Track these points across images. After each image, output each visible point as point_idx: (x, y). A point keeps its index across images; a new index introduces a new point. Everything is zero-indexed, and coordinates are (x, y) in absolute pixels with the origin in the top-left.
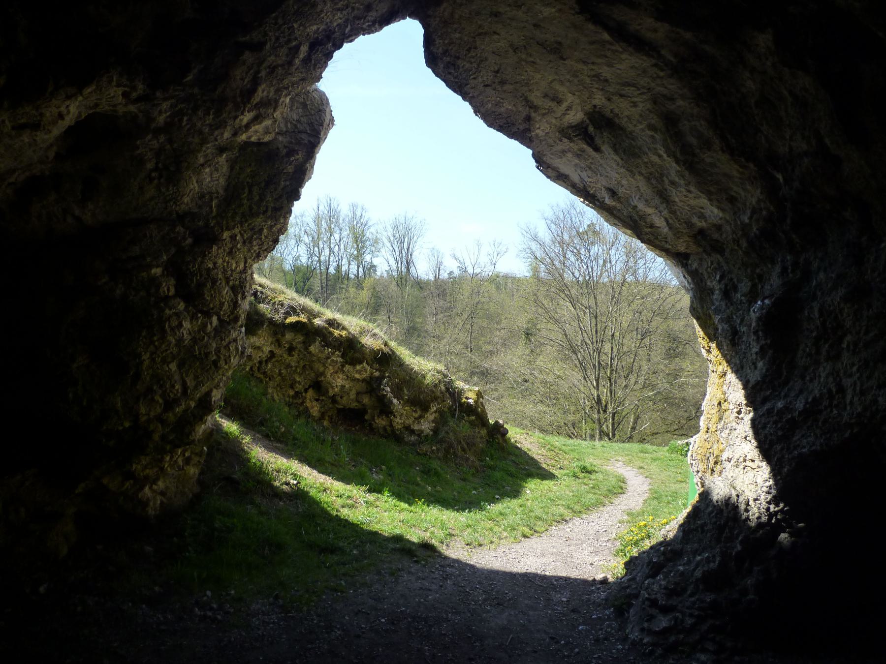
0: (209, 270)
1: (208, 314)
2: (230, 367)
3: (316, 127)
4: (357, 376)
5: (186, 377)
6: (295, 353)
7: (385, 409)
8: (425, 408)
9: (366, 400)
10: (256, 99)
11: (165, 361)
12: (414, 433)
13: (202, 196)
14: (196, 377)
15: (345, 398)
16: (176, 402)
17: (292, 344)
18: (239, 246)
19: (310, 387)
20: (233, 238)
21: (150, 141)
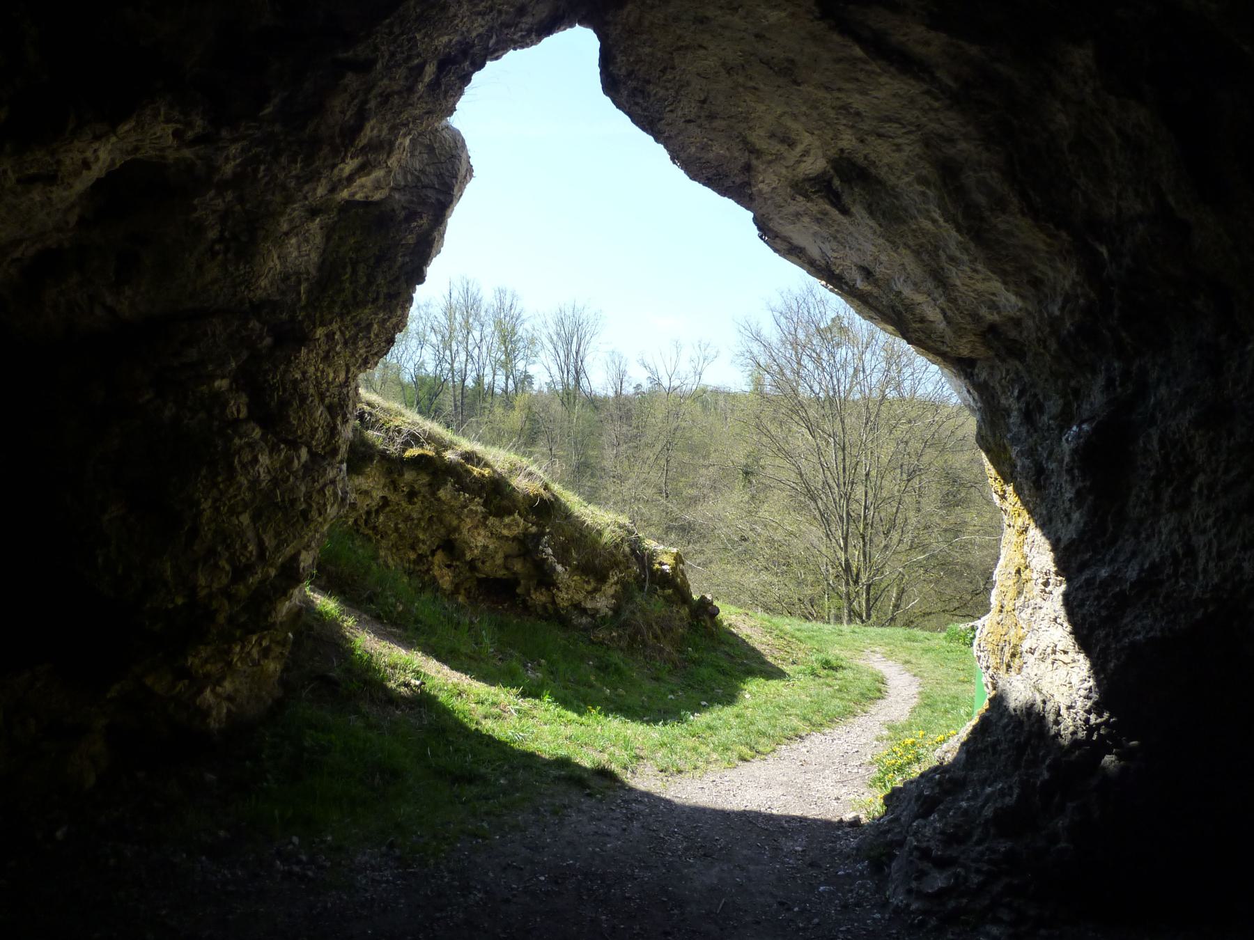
0: (295, 382)
1: (294, 445)
2: (325, 520)
3: (447, 180)
4: (505, 532)
6: (418, 500)
7: (545, 579)
8: (602, 578)
9: (518, 566)
10: (362, 140)
11: (233, 512)
14: (278, 534)
15: (488, 564)
16: (249, 569)
18: (338, 348)
19: (438, 547)
20: (330, 336)
21: (212, 199)
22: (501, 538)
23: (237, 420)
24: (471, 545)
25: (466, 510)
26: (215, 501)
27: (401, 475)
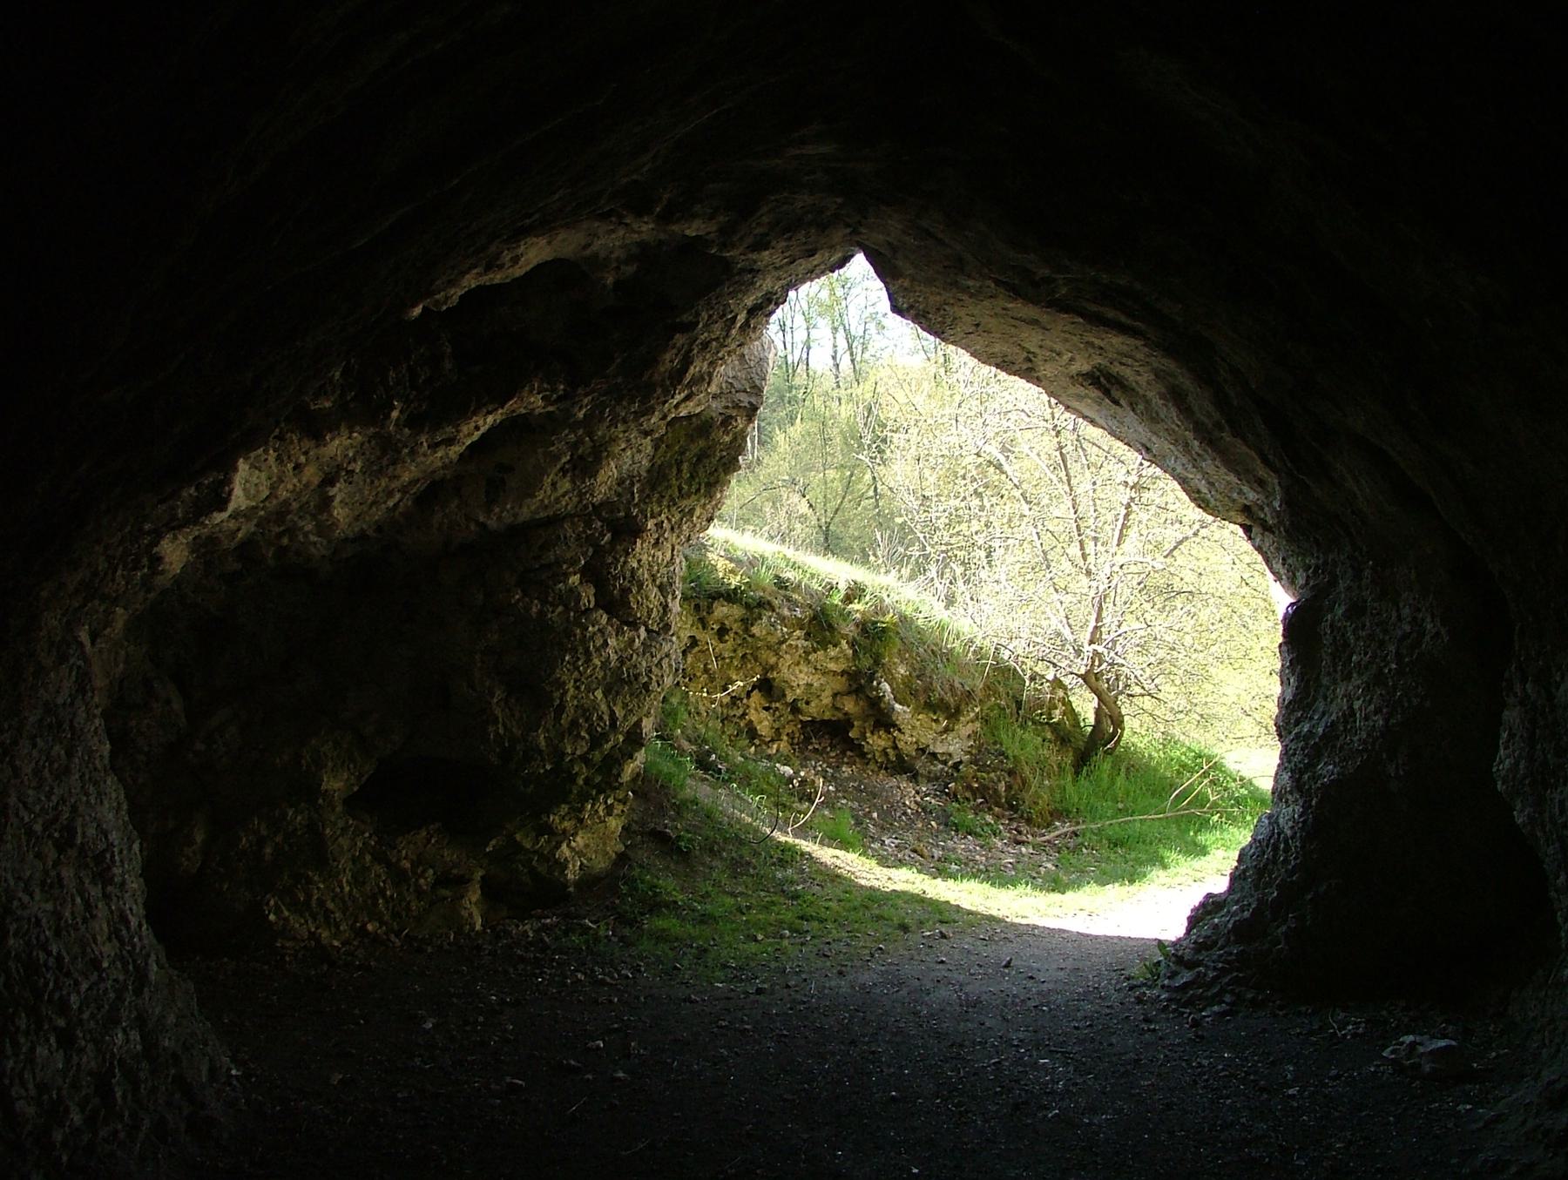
0: (633, 571)
1: (634, 625)
2: (663, 690)
3: (757, 382)
4: (832, 666)
5: (615, 705)
6: (729, 637)
7: (883, 721)
8: (954, 714)
9: (849, 705)
10: (688, 377)
11: (590, 690)
12: (937, 759)
13: (620, 482)
14: (625, 705)
15: (813, 704)
16: (604, 737)
17: (723, 624)
18: (666, 535)
19: (754, 687)
20: (659, 525)
21: (567, 435)
22: (825, 673)
23: (588, 610)
24: (793, 684)
25: (784, 646)
26: (576, 681)
27: (710, 611)
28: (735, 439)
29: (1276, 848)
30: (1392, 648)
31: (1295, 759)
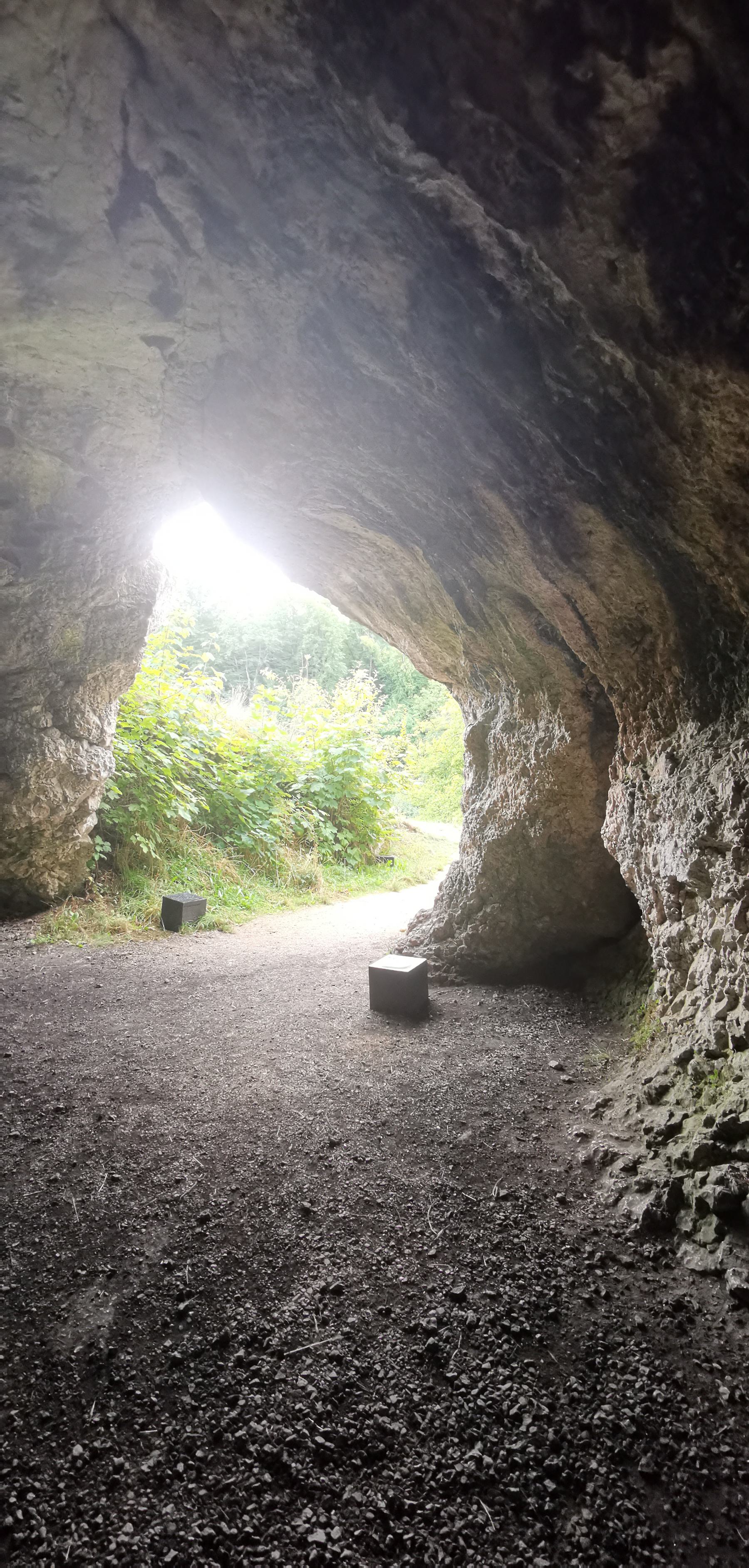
11: (47, 777)
23: (46, 728)
28: (139, 625)
29: (460, 883)
30: (533, 749)
31: (471, 826)
